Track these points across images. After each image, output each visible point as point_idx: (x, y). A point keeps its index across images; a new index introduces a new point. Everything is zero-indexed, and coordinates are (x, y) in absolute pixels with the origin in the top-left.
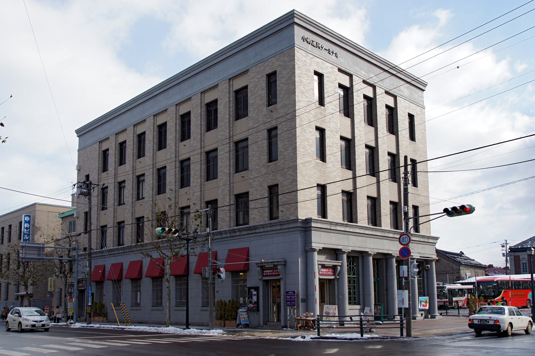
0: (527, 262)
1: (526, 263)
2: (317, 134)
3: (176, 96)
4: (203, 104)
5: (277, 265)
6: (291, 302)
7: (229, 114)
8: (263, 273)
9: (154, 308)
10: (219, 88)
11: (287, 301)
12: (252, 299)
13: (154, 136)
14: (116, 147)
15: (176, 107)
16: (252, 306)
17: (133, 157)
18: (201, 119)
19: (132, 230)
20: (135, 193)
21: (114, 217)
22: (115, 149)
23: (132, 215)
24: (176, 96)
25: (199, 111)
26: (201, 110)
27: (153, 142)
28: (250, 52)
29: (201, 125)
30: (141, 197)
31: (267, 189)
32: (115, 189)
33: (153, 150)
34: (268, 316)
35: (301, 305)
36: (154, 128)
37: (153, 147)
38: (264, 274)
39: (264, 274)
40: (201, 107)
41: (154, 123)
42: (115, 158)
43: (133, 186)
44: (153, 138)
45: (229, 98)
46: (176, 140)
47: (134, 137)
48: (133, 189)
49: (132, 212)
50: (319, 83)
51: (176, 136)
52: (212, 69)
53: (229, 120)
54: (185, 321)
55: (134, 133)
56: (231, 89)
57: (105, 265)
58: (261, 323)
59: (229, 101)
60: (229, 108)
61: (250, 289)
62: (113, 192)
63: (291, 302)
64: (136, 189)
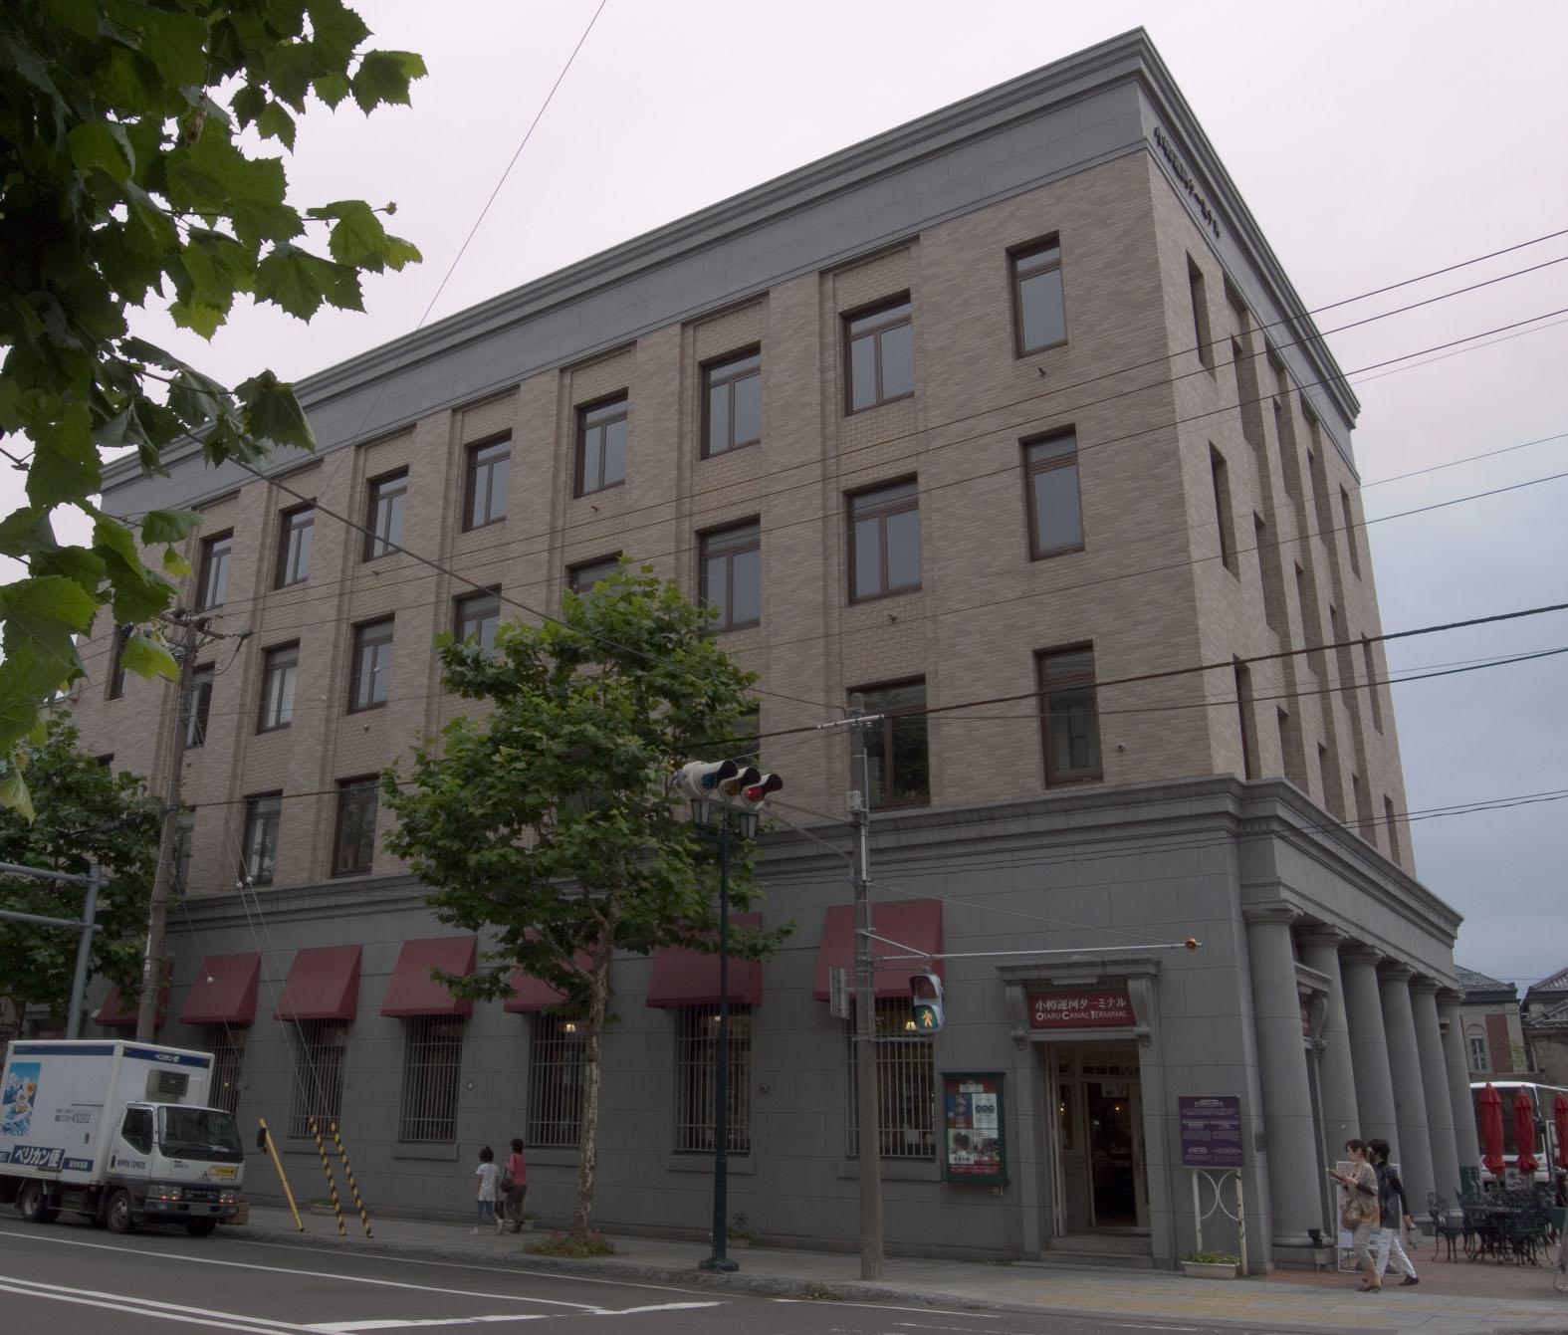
0: (1485, 1036)
1: (1481, 1041)
2: (584, 577)
3: (571, 335)
4: (689, 362)
5: (1124, 978)
6: (1212, 1145)
7: (823, 392)
8: (1032, 1011)
9: (407, 1149)
10: (772, 303)
11: (1187, 1144)
12: (969, 1124)
13: (448, 480)
14: (265, 523)
15: (561, 378)
16: (973, 1158)
17: (345, 558)
18: (681, 411)
19: (317, 825)
20: (342, 684)
21: (234, 776)
22: (264, 530)
23: (323, 771)
24: (571, 335)
25: (675, 386)
26: (681, 383)
27: (446, 498)
28: (923, 180)
29: (681, 435)
30: (271, 722)
31: (1030, 663)
32: (246, 671)
33: (443, 528)
34: (1051, 1207)
35: (1258, 1159)
36: (450, 453)
37: (444, 518)
38: (1040, 1017)
39: (1040, 1017)
40: (682, 372)
41: (452, 433)
42: (261, 560)
43: (334, 659)
44: (447, 488)
45: (821, 335)
46: (555, 491)
47: (353, 487)
48: (334, 670)
49: (324, 758)
50: (488, 447)
51: (555, 478)
52: (737, 247)
53: (823, 414)
54: (705, 1217)
55: (355, 471)
56: (829, 305)
57: (360, 951)
58: (1031, 1238)
59: (823, 346)
60: (823, 370)
61: (953, 1080)
62: (238, 683)
63: (1212, 1145)
64: (347, 671)
